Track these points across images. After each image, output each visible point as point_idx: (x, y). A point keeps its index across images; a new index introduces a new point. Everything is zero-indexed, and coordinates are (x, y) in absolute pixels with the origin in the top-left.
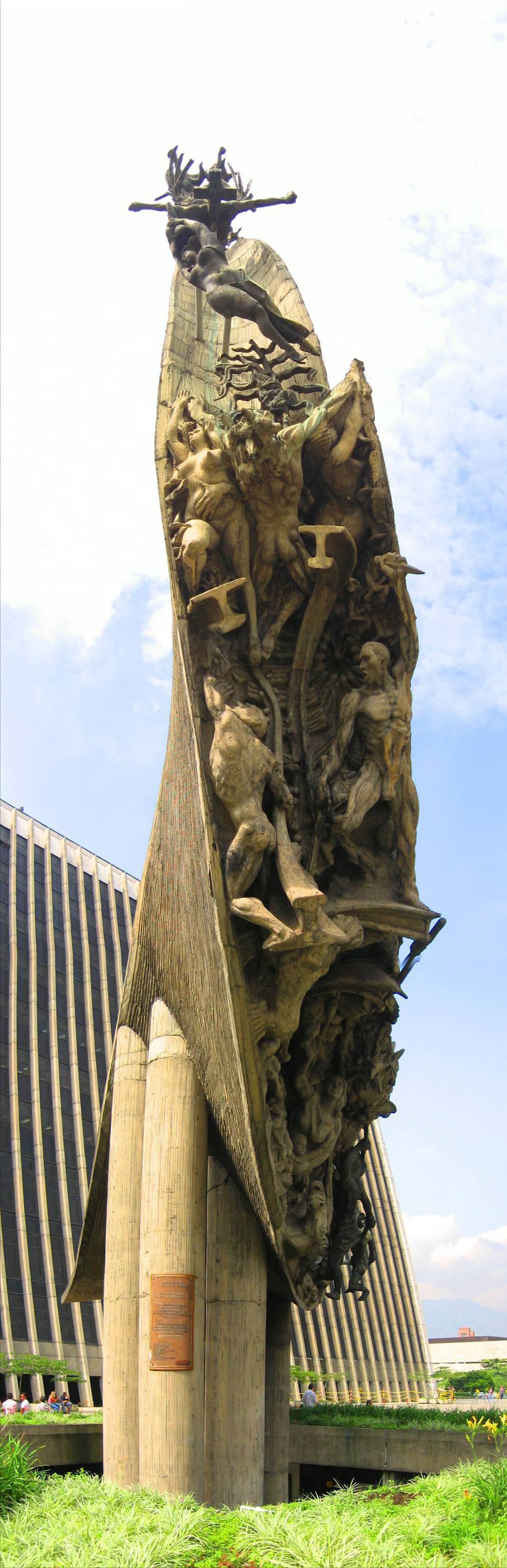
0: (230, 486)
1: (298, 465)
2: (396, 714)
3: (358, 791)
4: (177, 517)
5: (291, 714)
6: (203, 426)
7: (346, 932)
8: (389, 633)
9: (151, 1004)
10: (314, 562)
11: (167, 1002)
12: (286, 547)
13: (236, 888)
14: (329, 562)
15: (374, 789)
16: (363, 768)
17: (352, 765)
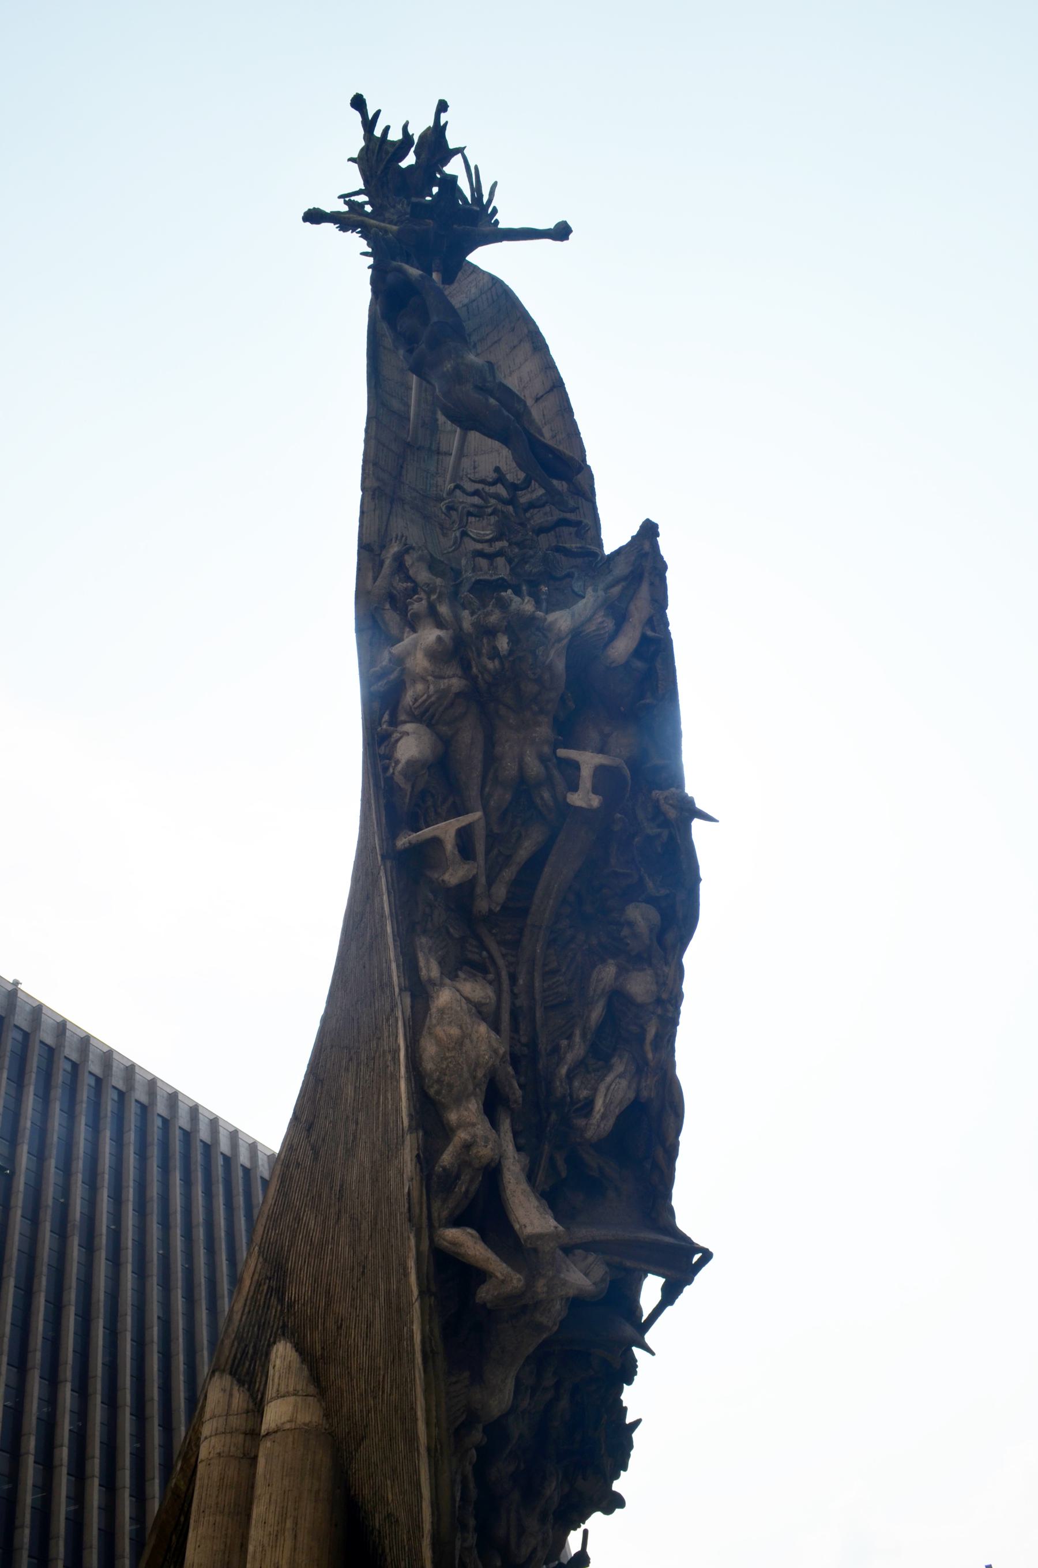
0: (464, 682)
1: (560, 665)
2: (665, 996)
3: (608, 1089)
4: (386, 717)
5: (521, 982)
6: (429, 594)
7: (586, 1275)
8: (663, 892)
9: (270, 1345)
10: (576, 799)
11: (299, 1348)
12: (534, 767)
13: (445, 1213)
14: (595, 801)
15: (629, 1087)
16: (615, 1060)
17: (599, 1056)
